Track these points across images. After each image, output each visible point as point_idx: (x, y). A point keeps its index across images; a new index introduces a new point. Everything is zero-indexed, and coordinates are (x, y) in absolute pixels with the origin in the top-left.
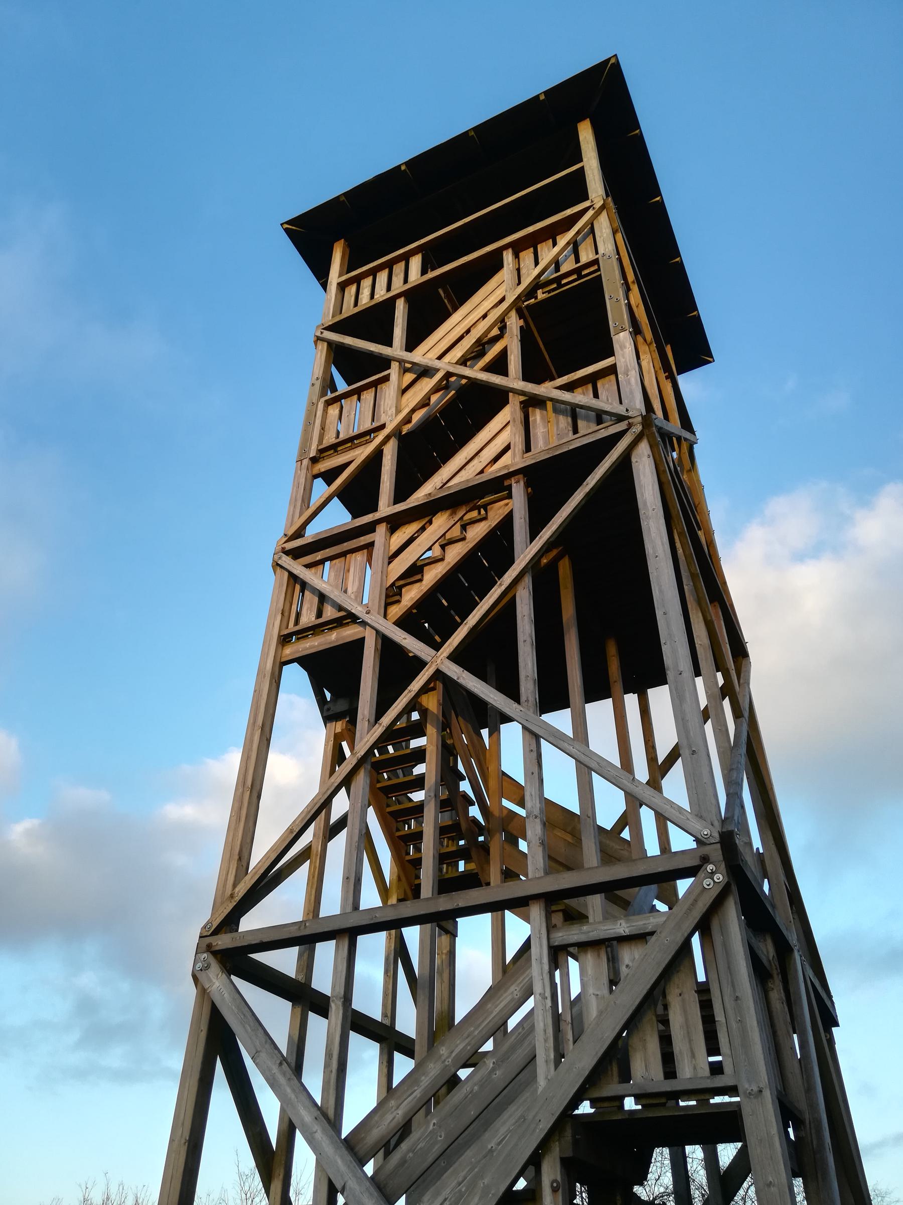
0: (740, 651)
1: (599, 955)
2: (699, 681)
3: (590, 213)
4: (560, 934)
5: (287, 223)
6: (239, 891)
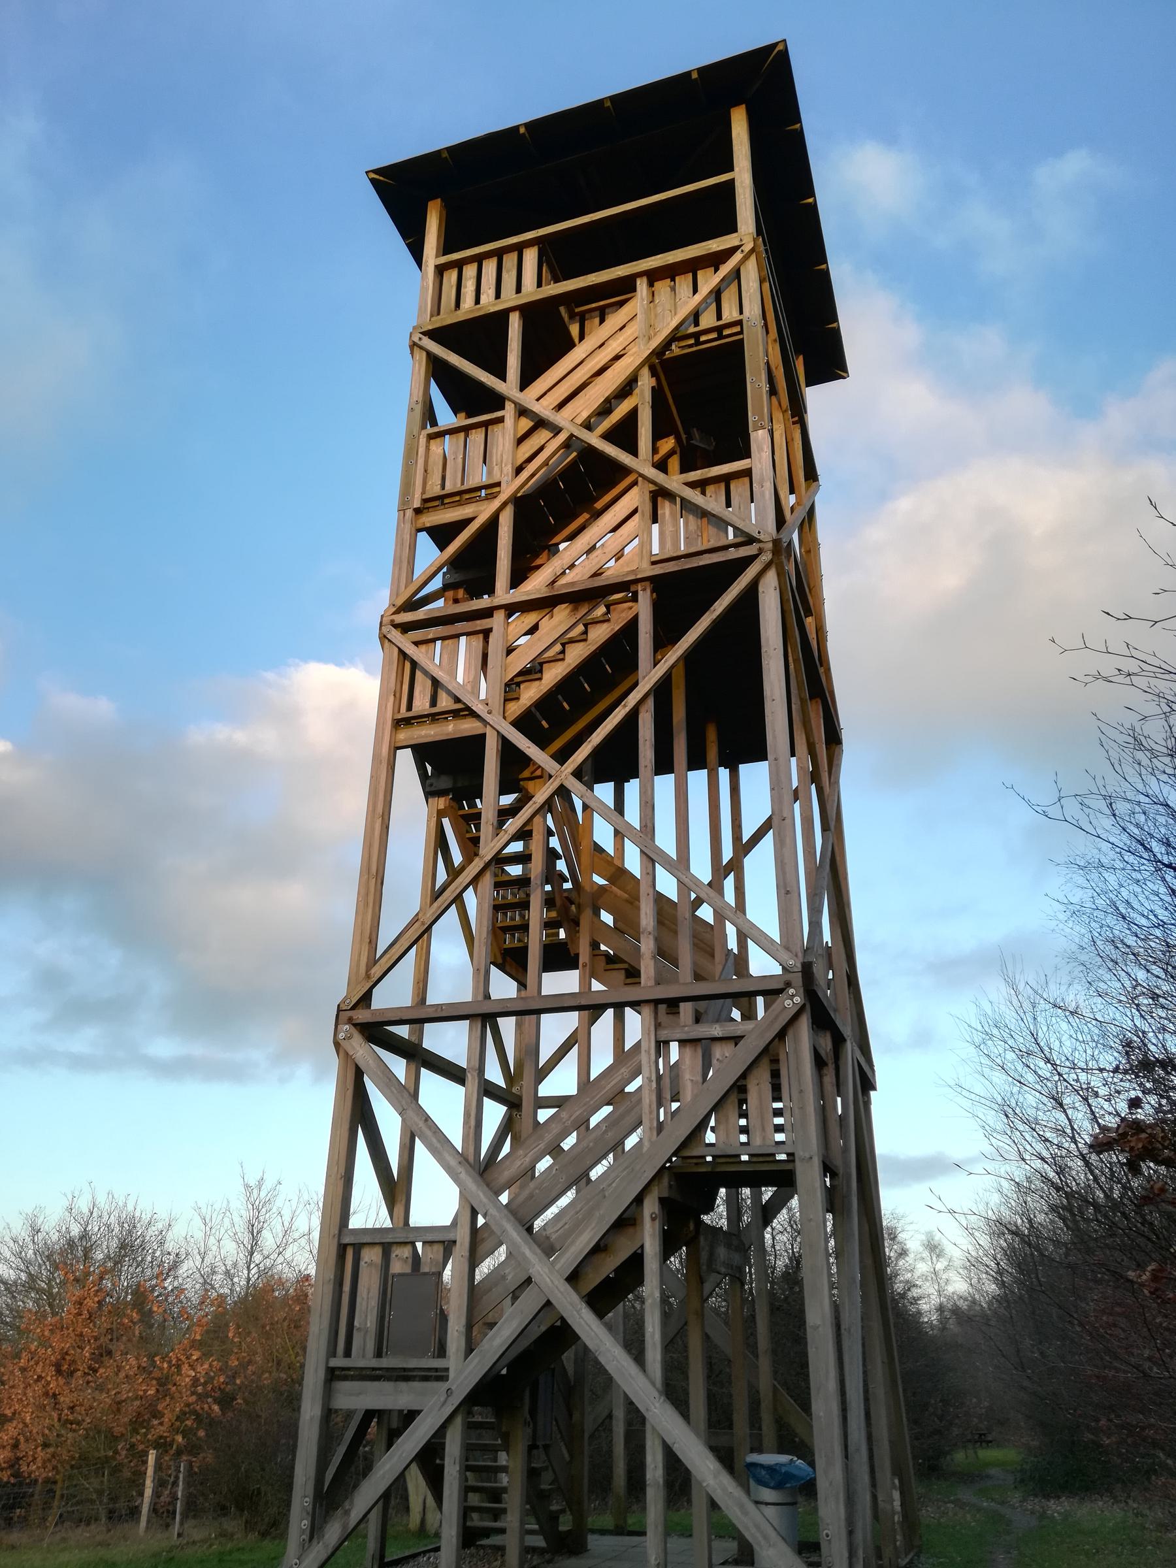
0: (834, 738)
1: (695, 1051)
2: (793, 760)
3: (738, 256)
4: (666, 1032)
5: (374, 171)
6: (375, 973)
